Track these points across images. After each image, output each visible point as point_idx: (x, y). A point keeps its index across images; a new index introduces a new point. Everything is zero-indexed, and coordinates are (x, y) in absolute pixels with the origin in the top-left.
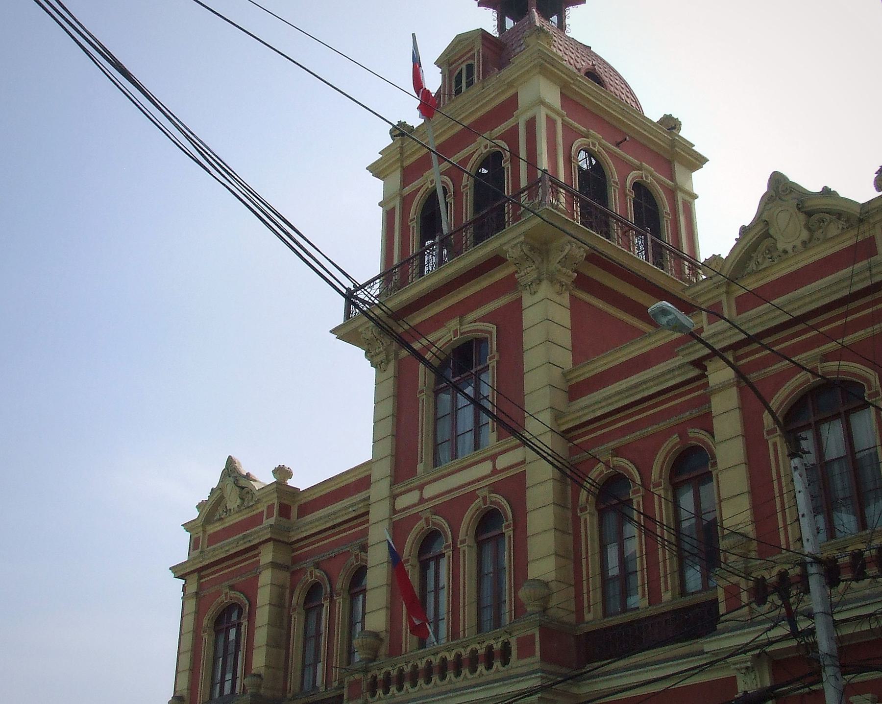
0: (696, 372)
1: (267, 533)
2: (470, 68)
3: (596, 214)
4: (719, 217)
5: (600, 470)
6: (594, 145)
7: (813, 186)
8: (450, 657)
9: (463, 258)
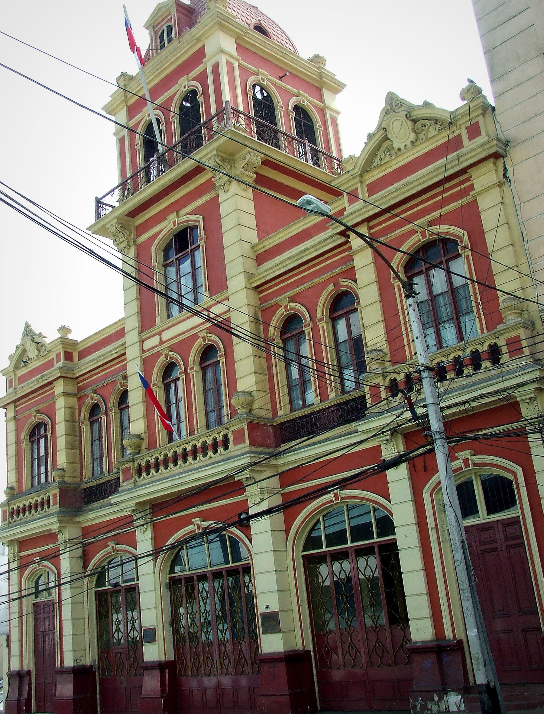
0: (343, 239)
1: (58, 373)
2: (169, 28)
3: (267, 131)
4: (353, 126)
5: (281, 313)
6: (263, 80)
7: (417, 101)
8: (189, 448)
9: (174, 169)
